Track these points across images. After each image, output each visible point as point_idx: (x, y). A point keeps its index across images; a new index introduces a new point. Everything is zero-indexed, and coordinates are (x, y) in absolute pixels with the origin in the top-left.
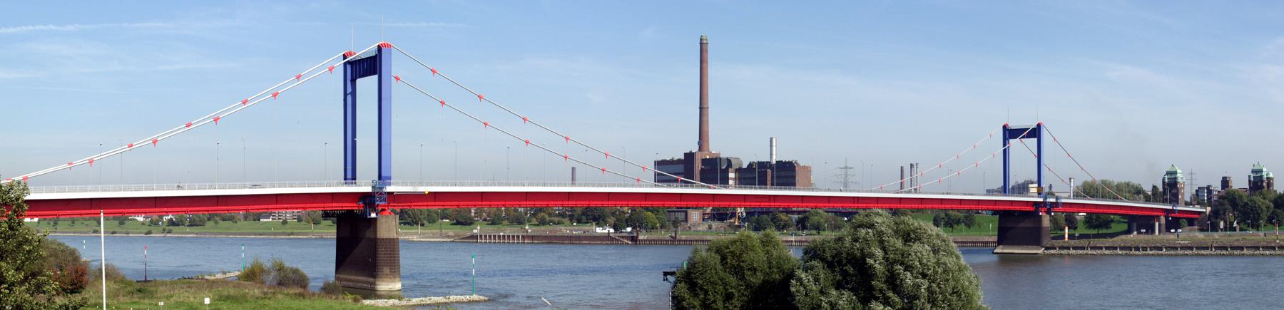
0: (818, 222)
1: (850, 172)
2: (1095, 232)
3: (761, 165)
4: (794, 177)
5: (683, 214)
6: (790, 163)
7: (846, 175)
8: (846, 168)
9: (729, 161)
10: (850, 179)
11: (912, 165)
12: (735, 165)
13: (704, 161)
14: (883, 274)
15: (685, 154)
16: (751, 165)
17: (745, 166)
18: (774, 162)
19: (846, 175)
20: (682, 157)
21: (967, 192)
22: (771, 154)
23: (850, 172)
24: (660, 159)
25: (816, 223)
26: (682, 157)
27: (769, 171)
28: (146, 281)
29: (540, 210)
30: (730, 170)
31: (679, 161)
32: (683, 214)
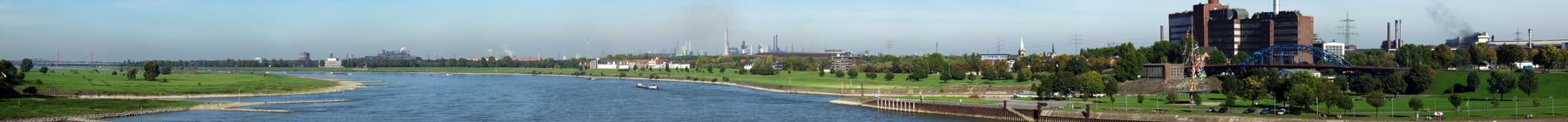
0: (1305, 94)
1: (1351, 24)
2: (1151, 64)
3: (1265, 16)
4: (1296, 27)
5: (1160, 70)
6: (1293, 13)
7: (1348, 27)
8: (1347, 20)
9: (1234, 12)
10: (1351, 31)
11: (1396, 21)
12: (1241, 16)
13: (1212, 13)
14: (1141, 69)
15: (1195, 7)
16: (1255, 16)
17: (1250, 17)
18: (1277, 13)
19: (1348, 27)
20: (1191, 9)
21: (497, 72)
22: (1275, 5)
23: (1351, 24)
24: (1174, 13)
25: (1300, 94)
26: (1191, 9)
27: (1272, 22)
28: (1347, 20)
29: (867, 70)
30: (1235, 21)
31: (1190, 14)
32: (1160, 70)
